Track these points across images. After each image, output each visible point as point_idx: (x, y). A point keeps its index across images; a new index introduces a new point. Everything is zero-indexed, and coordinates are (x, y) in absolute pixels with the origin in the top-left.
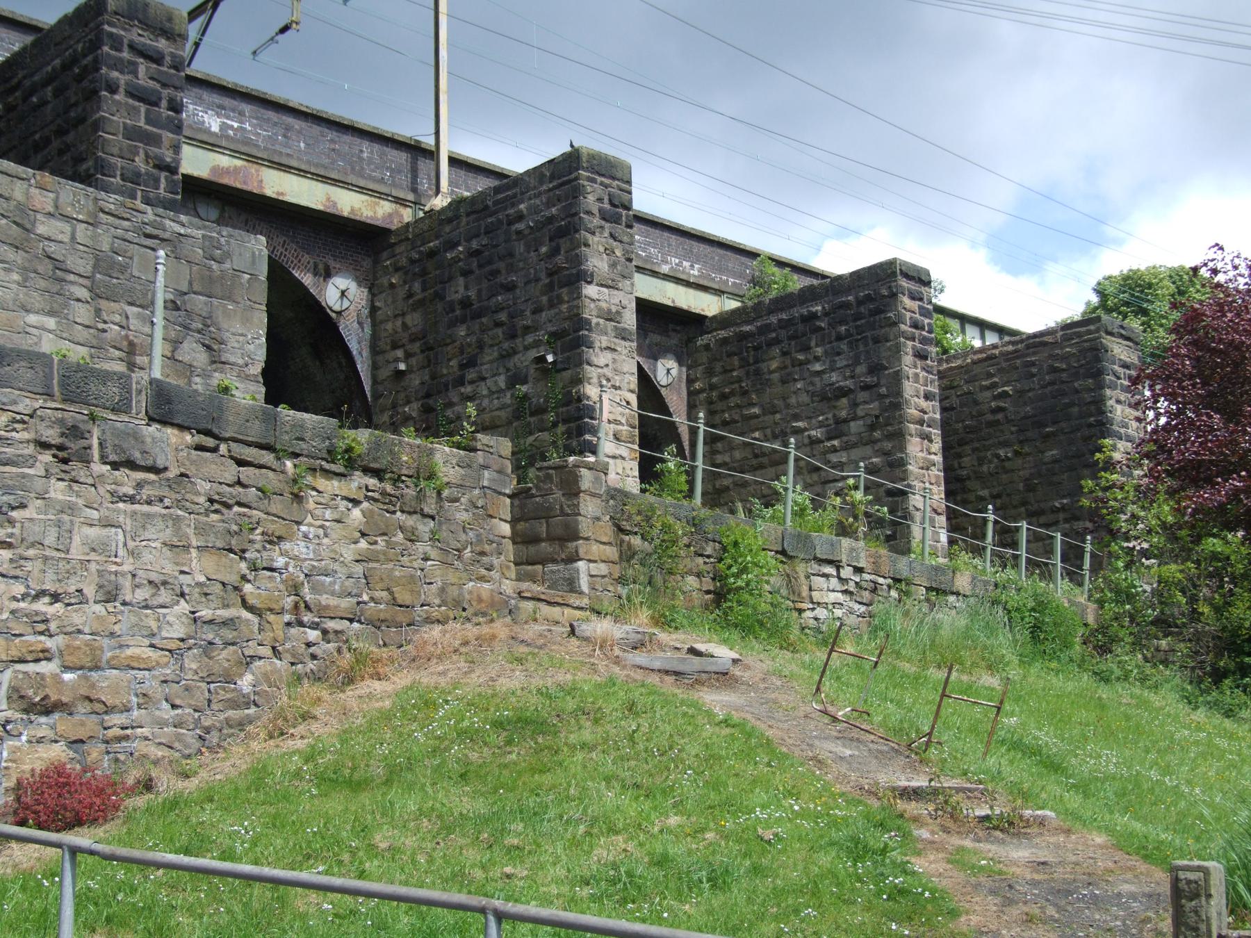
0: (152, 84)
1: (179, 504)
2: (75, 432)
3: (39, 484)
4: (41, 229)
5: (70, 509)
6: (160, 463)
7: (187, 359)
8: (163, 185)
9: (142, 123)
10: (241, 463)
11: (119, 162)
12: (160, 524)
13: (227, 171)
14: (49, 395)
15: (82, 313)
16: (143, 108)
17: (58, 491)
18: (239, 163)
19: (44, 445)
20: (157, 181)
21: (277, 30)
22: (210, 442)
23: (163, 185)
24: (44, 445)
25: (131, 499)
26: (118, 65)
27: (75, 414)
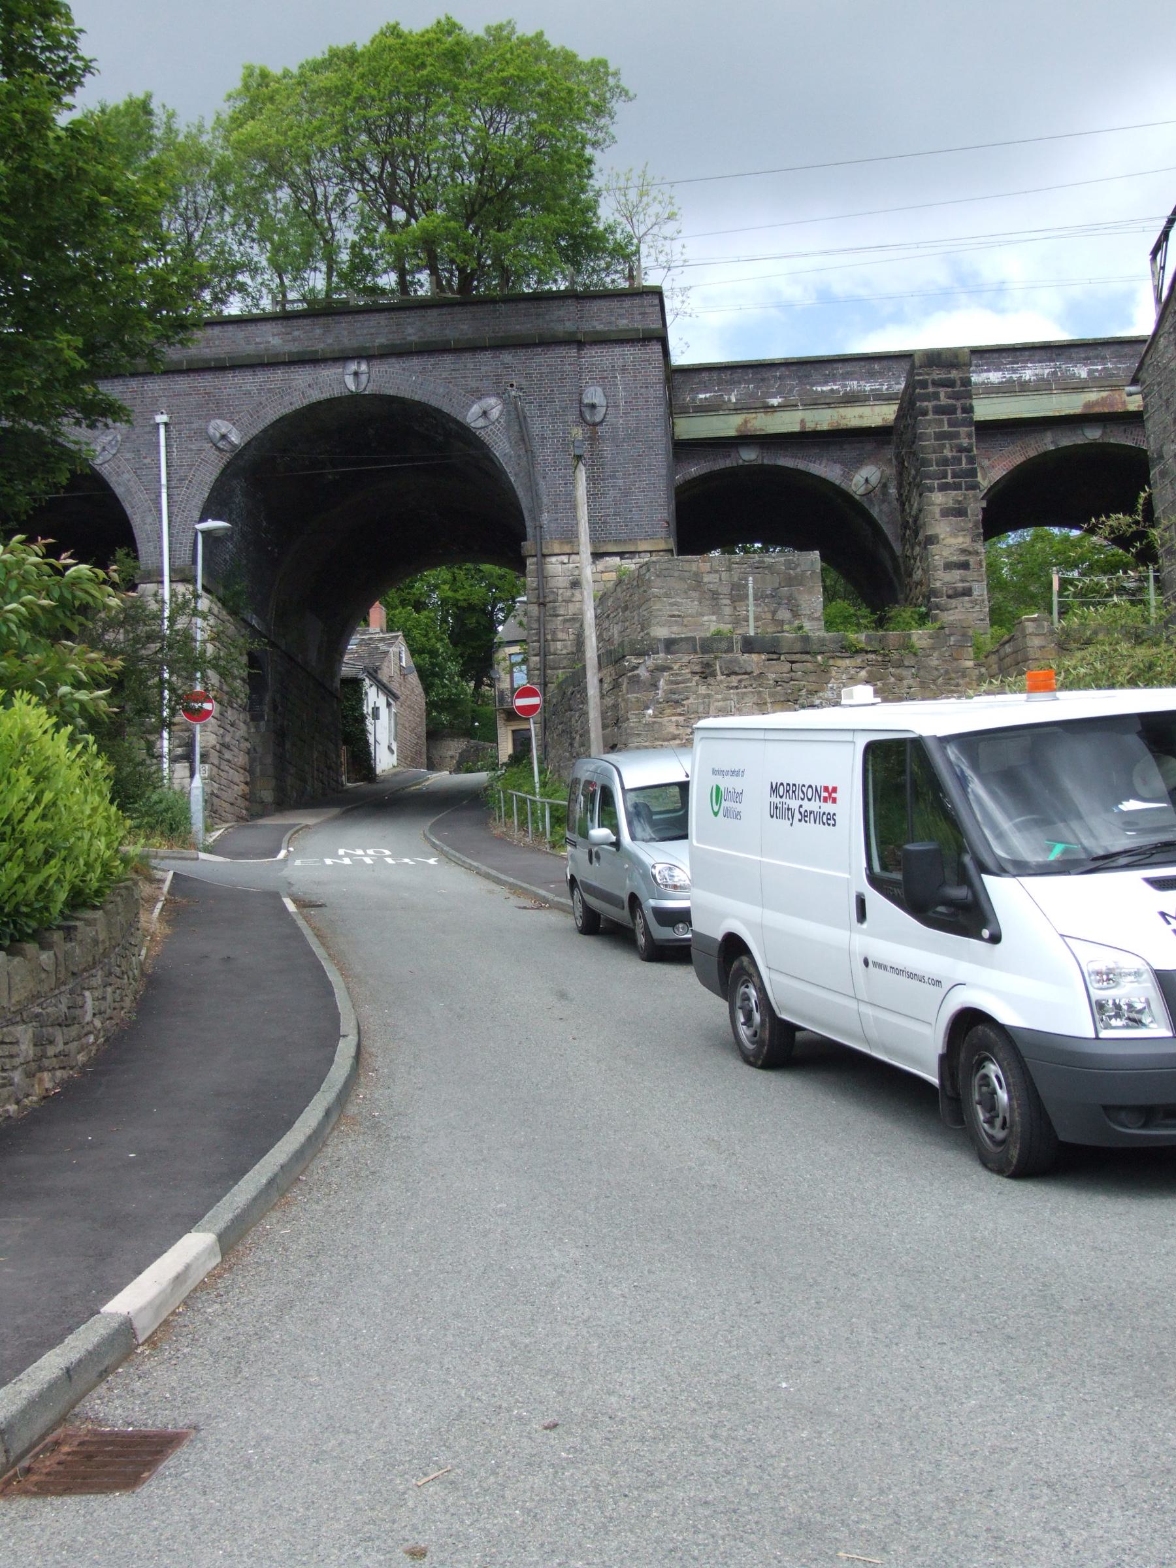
0: (950, 401)
1: (760, 686)
2: (708, 665)
3: (694, 689)
4: (705, 580)
5: (709, 696)
6: (749, 670)
7: (780, 618)
8: (964, 461)
9: (946, 428)
10: (792, 662)
11: (933, 456)
12: (750, 696)
13: (1096, 403)
14: (695, 652)
15: (727, 610)
16: (945, 418)
17: (703, 690)
18: (1104, 394)
19: (696, 673)
20: (960, 460)
21: (1149, 263)
22: (775, 656)
23: (964, 461)
24: (696, 673)
25: (737, 688)
26: (927, 397)
27: (707, 657)
